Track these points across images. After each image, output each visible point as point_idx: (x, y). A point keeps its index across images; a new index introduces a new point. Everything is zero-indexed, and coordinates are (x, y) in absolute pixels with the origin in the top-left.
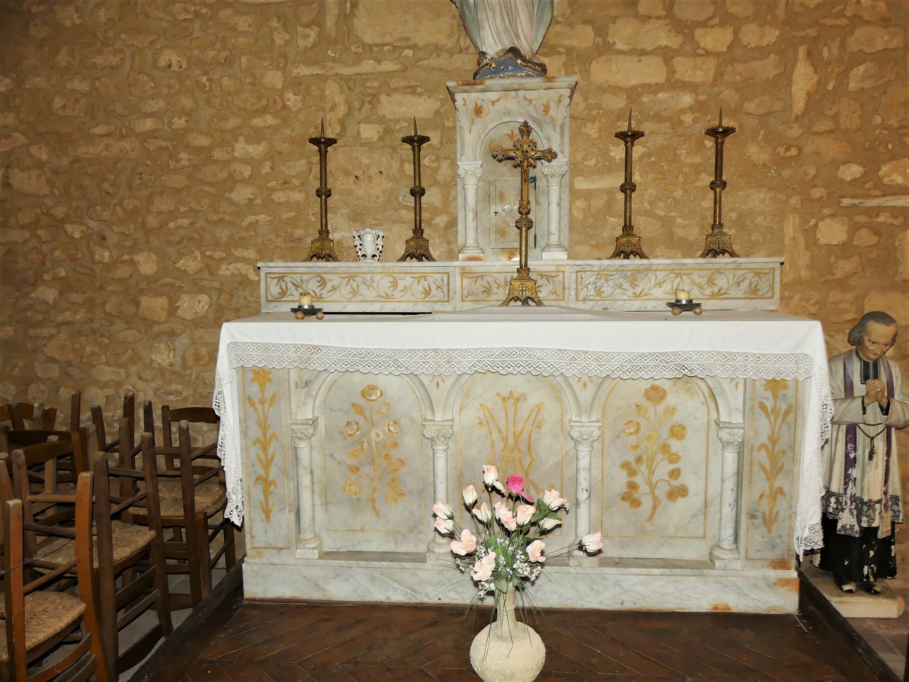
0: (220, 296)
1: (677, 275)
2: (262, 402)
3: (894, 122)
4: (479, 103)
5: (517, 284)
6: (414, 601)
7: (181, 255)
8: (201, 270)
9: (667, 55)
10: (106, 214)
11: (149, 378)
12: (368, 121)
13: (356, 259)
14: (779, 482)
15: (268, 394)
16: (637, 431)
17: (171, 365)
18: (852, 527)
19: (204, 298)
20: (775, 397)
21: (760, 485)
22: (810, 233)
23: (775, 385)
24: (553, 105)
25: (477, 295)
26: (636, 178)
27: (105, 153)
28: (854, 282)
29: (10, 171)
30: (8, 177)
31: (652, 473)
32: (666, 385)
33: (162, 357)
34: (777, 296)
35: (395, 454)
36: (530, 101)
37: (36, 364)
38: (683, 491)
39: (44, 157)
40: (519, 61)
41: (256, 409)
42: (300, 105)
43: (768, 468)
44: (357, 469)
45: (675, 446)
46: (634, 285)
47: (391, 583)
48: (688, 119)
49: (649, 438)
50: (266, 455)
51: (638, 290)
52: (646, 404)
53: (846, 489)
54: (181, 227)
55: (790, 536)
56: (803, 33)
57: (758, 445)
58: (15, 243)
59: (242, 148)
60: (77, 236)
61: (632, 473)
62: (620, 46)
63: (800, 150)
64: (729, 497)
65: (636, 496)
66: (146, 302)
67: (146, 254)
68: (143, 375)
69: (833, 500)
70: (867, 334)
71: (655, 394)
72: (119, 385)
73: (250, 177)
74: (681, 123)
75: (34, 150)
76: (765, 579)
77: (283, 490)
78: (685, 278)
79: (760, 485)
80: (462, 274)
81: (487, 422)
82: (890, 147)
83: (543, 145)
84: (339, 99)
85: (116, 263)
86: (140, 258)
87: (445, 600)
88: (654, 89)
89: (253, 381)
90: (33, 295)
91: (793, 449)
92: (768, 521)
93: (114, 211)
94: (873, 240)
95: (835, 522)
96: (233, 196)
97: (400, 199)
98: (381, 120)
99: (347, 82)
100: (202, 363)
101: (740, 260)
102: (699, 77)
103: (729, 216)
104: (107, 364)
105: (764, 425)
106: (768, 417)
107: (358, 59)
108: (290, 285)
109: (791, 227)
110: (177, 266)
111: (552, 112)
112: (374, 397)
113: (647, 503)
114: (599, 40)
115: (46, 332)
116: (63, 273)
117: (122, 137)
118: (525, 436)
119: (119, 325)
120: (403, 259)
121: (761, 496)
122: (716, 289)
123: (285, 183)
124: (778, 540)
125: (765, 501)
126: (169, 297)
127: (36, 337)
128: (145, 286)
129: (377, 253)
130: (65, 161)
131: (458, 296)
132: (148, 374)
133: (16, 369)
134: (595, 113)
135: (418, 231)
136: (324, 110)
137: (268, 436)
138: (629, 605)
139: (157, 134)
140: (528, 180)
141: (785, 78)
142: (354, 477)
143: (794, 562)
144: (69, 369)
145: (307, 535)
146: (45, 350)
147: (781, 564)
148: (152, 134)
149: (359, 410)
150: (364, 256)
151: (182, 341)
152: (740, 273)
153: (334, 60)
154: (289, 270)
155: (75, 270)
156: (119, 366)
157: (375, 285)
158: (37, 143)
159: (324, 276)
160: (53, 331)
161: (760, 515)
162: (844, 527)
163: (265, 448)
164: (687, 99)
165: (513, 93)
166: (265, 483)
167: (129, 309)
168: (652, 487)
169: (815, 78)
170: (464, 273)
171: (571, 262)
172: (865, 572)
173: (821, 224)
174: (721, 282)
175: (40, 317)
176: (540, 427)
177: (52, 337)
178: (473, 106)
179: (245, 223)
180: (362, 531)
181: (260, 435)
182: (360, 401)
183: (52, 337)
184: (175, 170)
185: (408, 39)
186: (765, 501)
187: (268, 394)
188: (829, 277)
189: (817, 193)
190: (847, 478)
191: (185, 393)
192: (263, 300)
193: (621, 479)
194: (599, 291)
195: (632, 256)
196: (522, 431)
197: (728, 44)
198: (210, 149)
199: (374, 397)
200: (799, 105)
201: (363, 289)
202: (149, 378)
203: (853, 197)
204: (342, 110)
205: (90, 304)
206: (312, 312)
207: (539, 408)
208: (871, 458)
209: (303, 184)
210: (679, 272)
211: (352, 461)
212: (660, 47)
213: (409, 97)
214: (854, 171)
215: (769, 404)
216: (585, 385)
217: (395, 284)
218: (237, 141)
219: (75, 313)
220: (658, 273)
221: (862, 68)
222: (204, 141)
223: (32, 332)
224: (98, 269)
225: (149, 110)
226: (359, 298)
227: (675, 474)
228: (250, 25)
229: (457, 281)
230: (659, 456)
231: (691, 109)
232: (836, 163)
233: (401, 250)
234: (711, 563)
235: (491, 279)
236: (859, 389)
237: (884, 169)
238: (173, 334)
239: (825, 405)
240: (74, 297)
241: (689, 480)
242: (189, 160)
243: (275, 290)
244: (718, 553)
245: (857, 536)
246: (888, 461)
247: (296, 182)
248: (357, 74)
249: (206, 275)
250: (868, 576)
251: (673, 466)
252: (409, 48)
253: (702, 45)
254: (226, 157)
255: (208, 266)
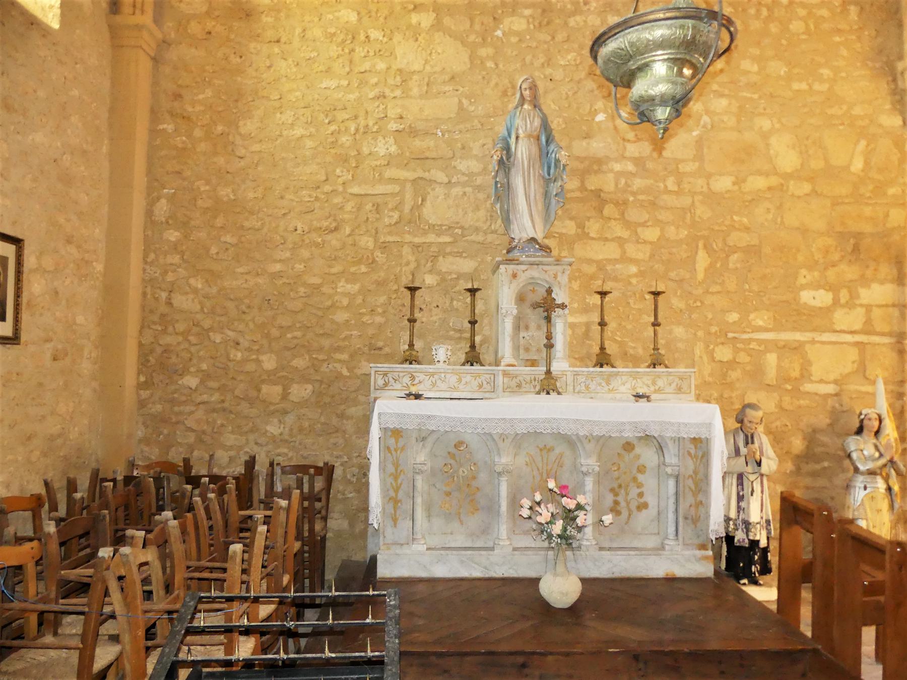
0: (321, 385)
1: (634, 379)
2: (396, 450)
3: (755, 288)
4: (515, 271)
5: (545, 382)
6: (487, 576)
7: (294, 357)
8: (308, 367)
9: (621, 241)
10: (241, 327)
11: (264, 443)
12: (430, 272)
13: (430, 364)
14: (700, 497)
15: (400, 444)
16: (619, 469)
17: (281, 434)
18: (744, 540)
19: (310, 387)
20: (696, 447)
21: (690, 499)
22: (711, 354)
23: (696, 441)
24: (559, 274)
25: (513, 388)
26: (606, 318)
27: (245, 286)
28: (738, 385)
29: (172, 294)
30: (170, 299)
31: (627, 494)
32: (635, 442)
33: (273, 429)
34: (693, 392)
35: (474, 484)
36: (546, 271)
37: (178, 432)
38: (645, 506)
39: (200, 286)
40: (537, 246)
41: (392, 454)
42: (385, 260)
43: (693, 488)
44: (450, 494)
45: (640, 477)
46: (608, 384)
47: (473, 565)
48: (634, 281)
49: (625, 473)
50: (397, 484)
51: (611, 387)
52: (623, 452)
53: (739, 516)
54: (295, 338)
55: (708, 530)
56: (701, 233)
57: (687, 476)
58: (170, 345)
59: (344, 286)
60: (218, 341)
61: (616, 495)
62: (592, 235)
63: (702, 303)
64: (672, 507)
65: (619, 508)
66: (265, 388)
67: (269, 355)
68: (259, 442)
69: (731, 523)
70: (746, 416)
71: (628, 446)
72: (240, 448)
73: (348, 305)
74: (630, 283)
75: (192, 281)
76: (695, 556)
77: (406, 506)
78: (638, 380)
79: (690, 499)
80: (504, 375)
81: (531, 464)
82: (754, 303)
83: (559, 301)
84: (411, 258)
85: (245, 361)
86: (263, 358)
87: (506, 575)
88: (616, 261)
89: (391, 436)
90: (180, 382)
91: (707, 478)
92: (695, 521)
93: (247, 325)
94: (748, 359)
95: (733, 538)
96: (335, 317)
97: (451, 324)
98: (439, 273)
99: (416, 247)
100: (305, 432)
101: (670, 370)
102: (640, 256)
103: (661, 342)
104: (232, 432)
105: (690, 465)
106: (692, 459)
107: (425, 233)
108: (391, 379)
109: (699, 349)
110: (291, 364)
111: (559, 279)
112: (462, 448)
113: (625, 514)
114: (579, 230)
115: (188, 409)
116: (204, 366)
117: (258, 274)
118: (554, 471)
119: (244, 405)
120: (463, 364)
121: (691, 506)
122: (657, 388)
123: (372, 311)
124: (701, 533)
125: (692, 509)
126: (283, 385)
127: (180, 413)
128: (266, 378)
129: (447, 360)
130: (214, 290)
131: (501, 389)
132: (262, 440)
133: (161, 436)
134: (577, 274)
135: (473, 347)
136: (401, 264)
137: (399, 471)
138: (617, 575)
139: (282, 274)
140: (548, 319)
141: (691, 260)
142: (448, 498)
143: (710, 545)
144: (203, 436)
145: (419, 536)
146: (186, 422)
147: (703, 547)
148: (279, 275)
149: (452, 455)
150: (438, 361)
151: (290, 419)
152: (671, 378)
153: (409, 232)
154: (391, 370)
155: (214, 365)
156: (241, 434)
157: (447, 380)
158: (194, 276)
159: (414, 374)
160: (193, 408)
161: (690, 517)
162: (739, 541)
163: (396, 479)
164: (634, 269)
165: (536, 266)
166: (395, 501)
167: (254, 393)
168: (628, 503)
169: (709, 260)
170: (505, 374)
171: (571, 369)
172: (753, 570)
173: (716, 348)
174: (660, 383)
175: (184, 398)
176: (562, 467)
177: (192, 413)
178: (511, 272)
179: (343, 336)
180: (452, 534)
181: (393, 470)
182: (453, 450)
183: (192, 413)
184: (294, 299)
185: (458, 223)
186: (692, 509)
187: (400, 444)
188: (724, 381)
189: (714, 329)
190: (739, 508)
191: (290, 454)
192: (372, 388)
193: (609, 499)
194: (587, 387)
195: (605, 366)
196: (551, 470)
197: (657, 237)
198: (321, 285)
199: (462, 448)
200: (700, 276)
201: (439, 382)
202: (264, 443)
203: (734, 333)
204: (413, 266)
205: (222, 389)
206: (418, 397)
207: (561, 455)
208: (752, 495)
209: (384, 312)
210: (635, 376)
211: (448, 489)
212: (617, 237)
213: (458, 259)
214: (734, 317)
215: (693, 451)
216: (590, 441)
217: (460, 380)
218: (340, 281)
219: (211, 395)
220: (623, 377)
221: (736, 255)
222: (316, 280)
223: (176, 409)
224: (231, 365)
225: (278, 257)
226: (435, 388)
227: (641, 495)
228: (353, 207)
229: (500, 379)
230: (632, 484)
231: (636, 275)
232: (724, 311)
233: (463, 358)
234: (663, 548)
235: (521, 379)
236: (744, 450)
237: (752, 316)
238: (285, 412)
239: (723, 452)
240: (213, 384)
241: (650, 499)
242: (305, 293)
243: (380, 382)
244: (666, 542)
245: (747, 546)
246: (762, 497)
247: (380, 310)
248: (424, 243)
249: (312, 371)
250: (755, 574)
251: (639, 490)
252: (459, 228)
253: (642, 237)
254: (331, 291)
255: (313, 365)
